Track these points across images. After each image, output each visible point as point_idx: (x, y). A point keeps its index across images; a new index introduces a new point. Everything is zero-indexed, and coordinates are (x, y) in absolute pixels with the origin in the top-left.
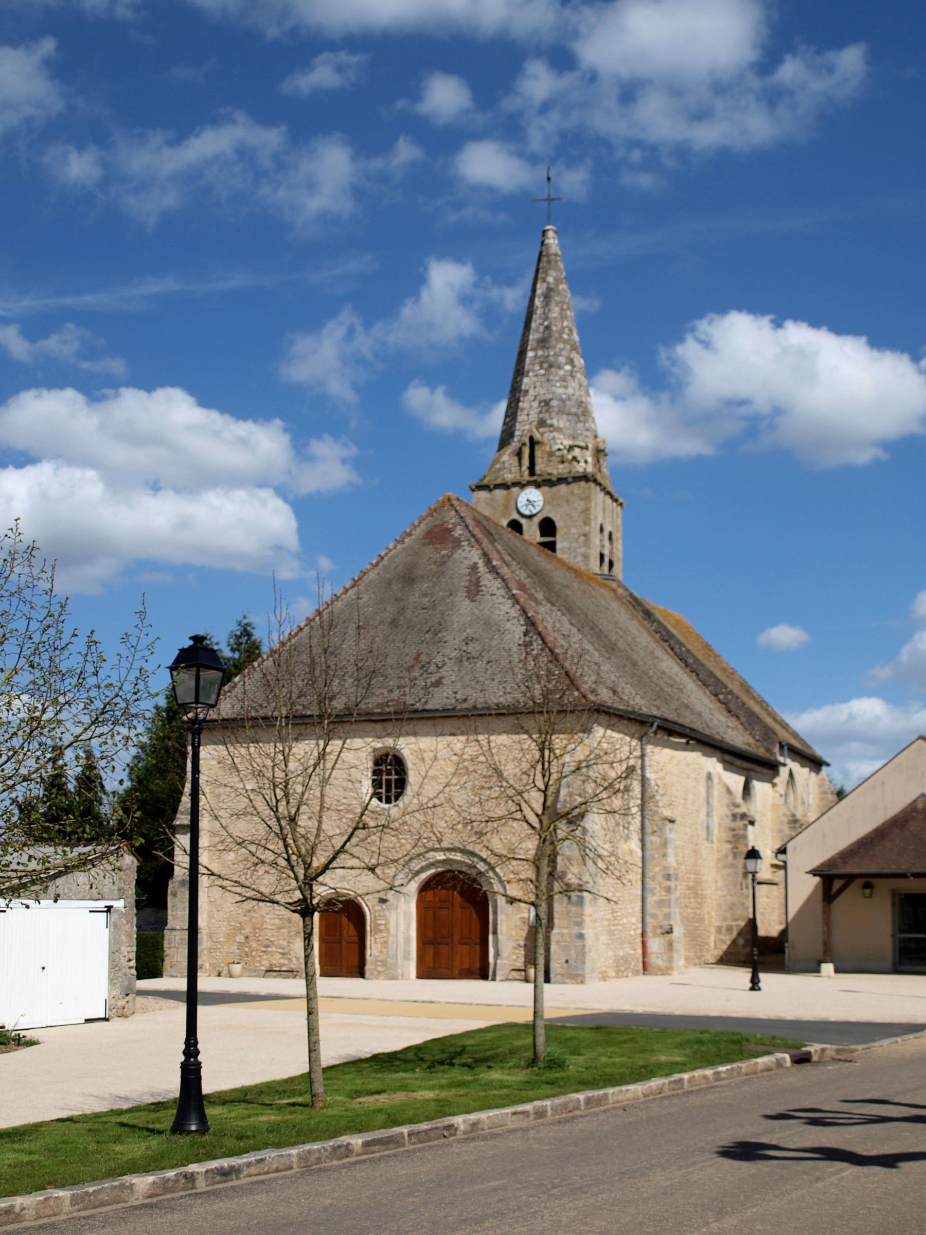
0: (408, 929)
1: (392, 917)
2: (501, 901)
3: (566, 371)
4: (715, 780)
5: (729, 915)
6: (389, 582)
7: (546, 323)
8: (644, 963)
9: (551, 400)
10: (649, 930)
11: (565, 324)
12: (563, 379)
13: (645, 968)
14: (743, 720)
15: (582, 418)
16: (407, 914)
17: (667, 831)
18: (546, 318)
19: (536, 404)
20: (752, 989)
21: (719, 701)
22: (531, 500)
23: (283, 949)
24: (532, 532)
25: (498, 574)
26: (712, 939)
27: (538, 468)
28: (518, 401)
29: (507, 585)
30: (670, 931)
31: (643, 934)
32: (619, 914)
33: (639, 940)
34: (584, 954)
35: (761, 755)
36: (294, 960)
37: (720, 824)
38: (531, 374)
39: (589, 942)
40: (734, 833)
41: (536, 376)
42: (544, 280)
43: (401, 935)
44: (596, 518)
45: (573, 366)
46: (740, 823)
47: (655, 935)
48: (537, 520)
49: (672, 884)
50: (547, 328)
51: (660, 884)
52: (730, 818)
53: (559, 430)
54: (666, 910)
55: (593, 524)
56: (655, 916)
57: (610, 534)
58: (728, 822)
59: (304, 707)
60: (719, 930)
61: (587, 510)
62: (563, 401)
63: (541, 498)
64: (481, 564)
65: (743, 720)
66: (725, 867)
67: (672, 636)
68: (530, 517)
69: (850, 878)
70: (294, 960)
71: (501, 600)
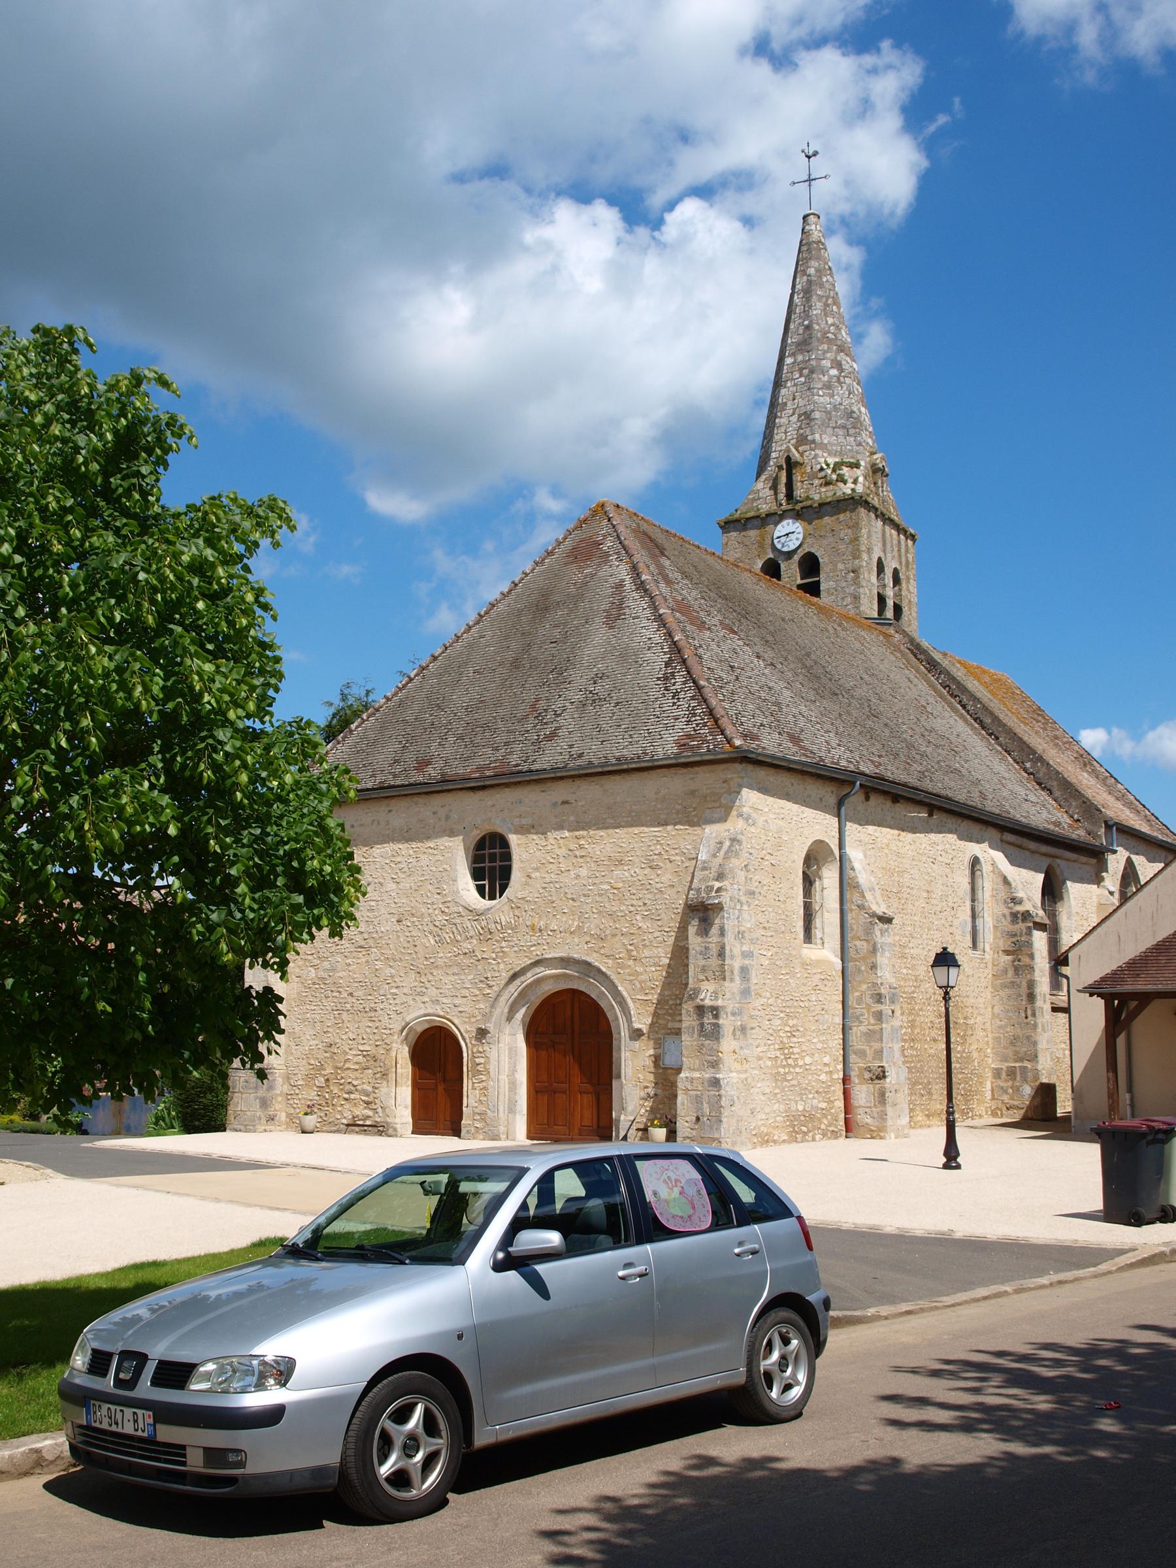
0: (513, 1070)
1: (493, 1054)
2: (624, 1033)
3: (831, 377)
4: (986, 868)
5: (1010, 1052)
6: (520, 611)
7: (806, 323)
8: (847, 1121)
9: (813, 411)
10: (854, 1074)
11: (830, 321)
12: (828, 386)
13: (849, 1128)
14: (1057, 793)
15: (852, 431)
16: (512, 1051)
17: (878, 933)
18: (808, 316)
19: (794, 418)
20: (946, 1166)
21: (1025, 770)
22: (790, 534)
23: (368, 1095)
24: (791, 572)
25: (646, 591)
26: (988, 1086)
27: (799, 492)
28: (776, 417)
29: (654, 603)
30: (882, 1076)
31: (846, 1080)
32: (796, 1050)
33: (839, 1088)
34: (716, 1106)
35: (1082, 839)
36: (380, 1110)
37: (995, 927)
38: (789, 384)
39: (728, 1091)
40: (1014, 940)
41: (795, 385)
42: (804, 273)
43: (504, 1078)
44: (869, 551)
45: (841, 370)
46: (1021, 926)
47: (863, 1081)
48: (796, 558)
49: (886, 1008)
50: (808, 328)
51: (869, 1007)
52: (1009, 919)
53: (823, 447)
54: (876, 1045)
55: (865, 556)
56: (862, 1054)
57: (896, 573)
58: (1006, 924)
59: (395, 776)
60: (997, 1073)
61: (855, 540)
62: (828, 413)
63: (800, 530)
64: (629, 585)
65: (1057, 793)
66: (1003, 986)
67: (963, 689)
68: (789, 555)
69: (1145, 999)
70: (380, 1110)
71: (645, 623)
